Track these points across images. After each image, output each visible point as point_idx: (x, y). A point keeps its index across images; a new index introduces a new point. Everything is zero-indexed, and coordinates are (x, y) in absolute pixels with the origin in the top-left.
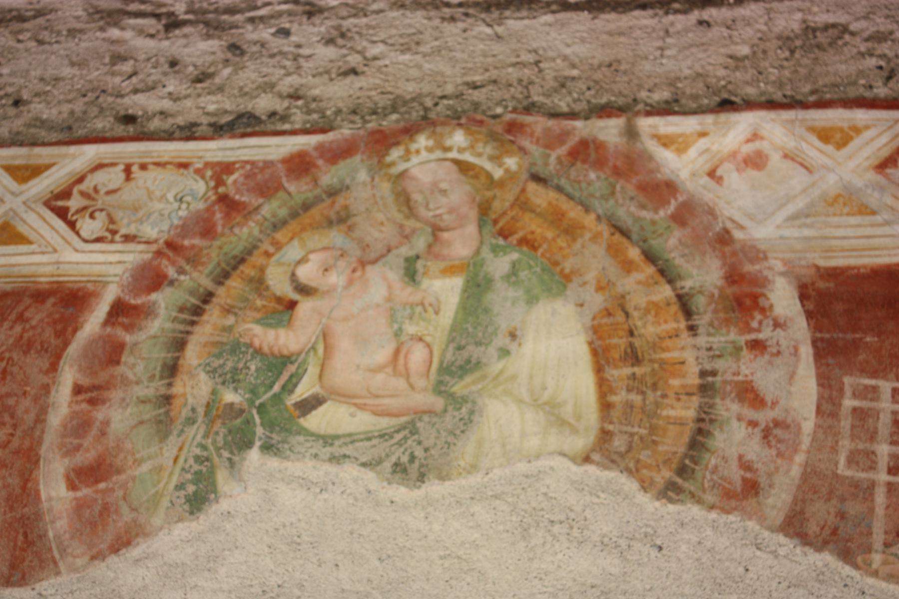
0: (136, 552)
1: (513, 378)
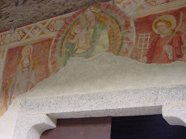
0: (58, 72)
1: (99, 42)
